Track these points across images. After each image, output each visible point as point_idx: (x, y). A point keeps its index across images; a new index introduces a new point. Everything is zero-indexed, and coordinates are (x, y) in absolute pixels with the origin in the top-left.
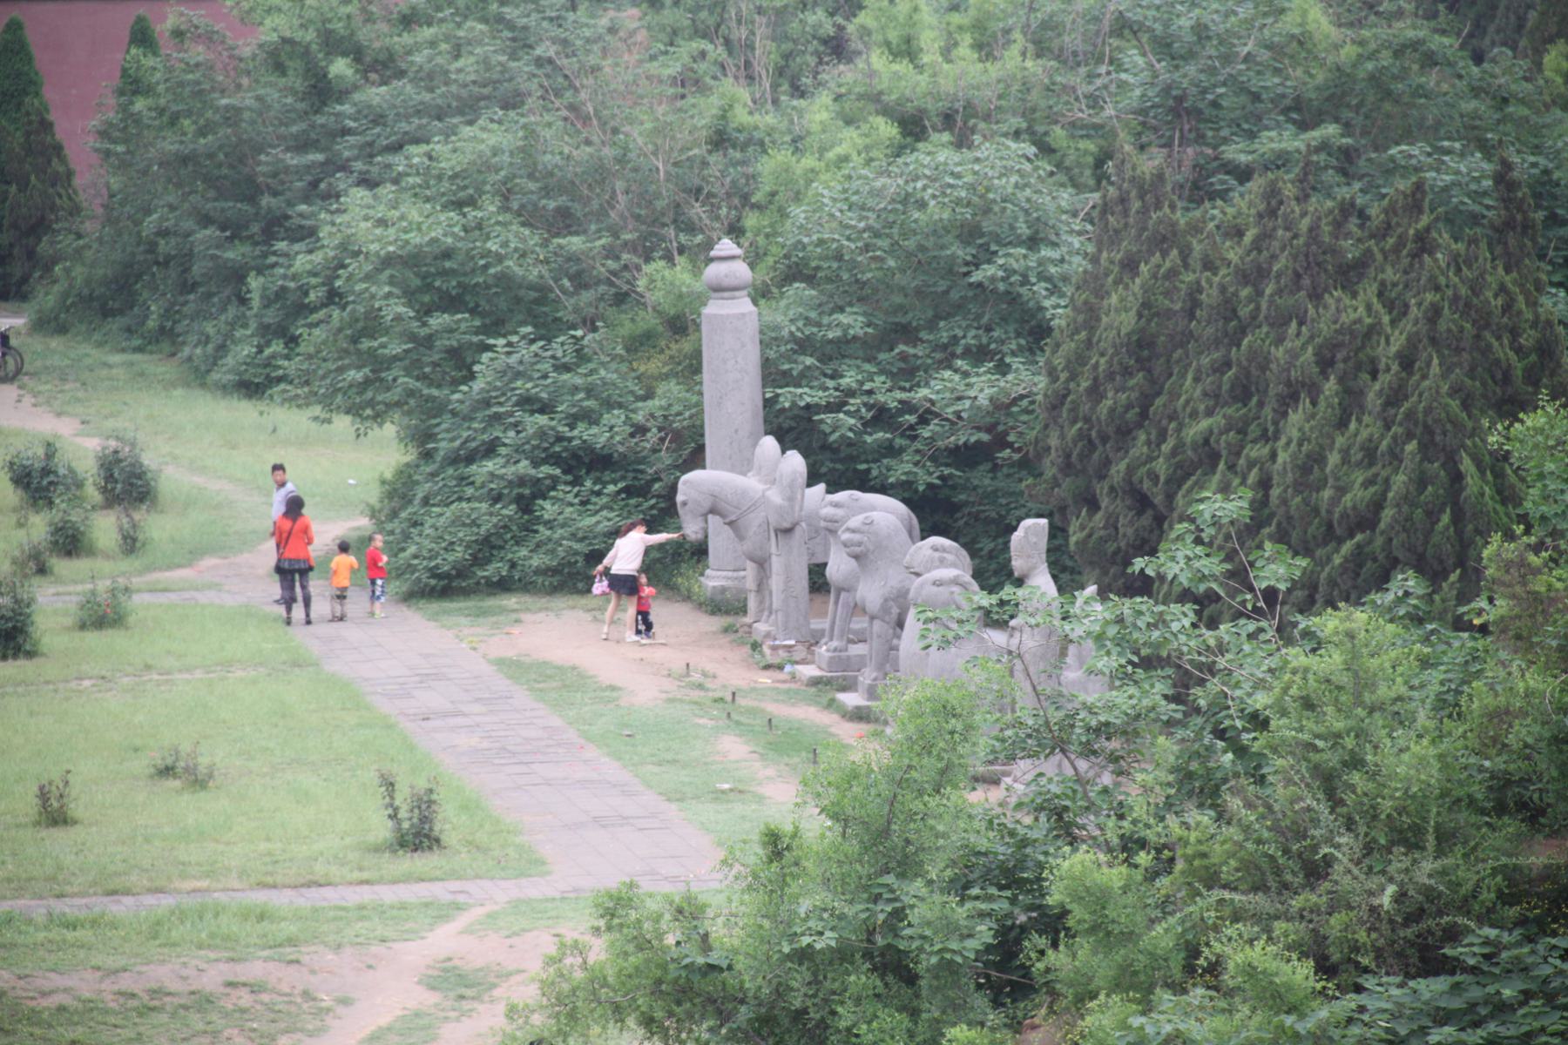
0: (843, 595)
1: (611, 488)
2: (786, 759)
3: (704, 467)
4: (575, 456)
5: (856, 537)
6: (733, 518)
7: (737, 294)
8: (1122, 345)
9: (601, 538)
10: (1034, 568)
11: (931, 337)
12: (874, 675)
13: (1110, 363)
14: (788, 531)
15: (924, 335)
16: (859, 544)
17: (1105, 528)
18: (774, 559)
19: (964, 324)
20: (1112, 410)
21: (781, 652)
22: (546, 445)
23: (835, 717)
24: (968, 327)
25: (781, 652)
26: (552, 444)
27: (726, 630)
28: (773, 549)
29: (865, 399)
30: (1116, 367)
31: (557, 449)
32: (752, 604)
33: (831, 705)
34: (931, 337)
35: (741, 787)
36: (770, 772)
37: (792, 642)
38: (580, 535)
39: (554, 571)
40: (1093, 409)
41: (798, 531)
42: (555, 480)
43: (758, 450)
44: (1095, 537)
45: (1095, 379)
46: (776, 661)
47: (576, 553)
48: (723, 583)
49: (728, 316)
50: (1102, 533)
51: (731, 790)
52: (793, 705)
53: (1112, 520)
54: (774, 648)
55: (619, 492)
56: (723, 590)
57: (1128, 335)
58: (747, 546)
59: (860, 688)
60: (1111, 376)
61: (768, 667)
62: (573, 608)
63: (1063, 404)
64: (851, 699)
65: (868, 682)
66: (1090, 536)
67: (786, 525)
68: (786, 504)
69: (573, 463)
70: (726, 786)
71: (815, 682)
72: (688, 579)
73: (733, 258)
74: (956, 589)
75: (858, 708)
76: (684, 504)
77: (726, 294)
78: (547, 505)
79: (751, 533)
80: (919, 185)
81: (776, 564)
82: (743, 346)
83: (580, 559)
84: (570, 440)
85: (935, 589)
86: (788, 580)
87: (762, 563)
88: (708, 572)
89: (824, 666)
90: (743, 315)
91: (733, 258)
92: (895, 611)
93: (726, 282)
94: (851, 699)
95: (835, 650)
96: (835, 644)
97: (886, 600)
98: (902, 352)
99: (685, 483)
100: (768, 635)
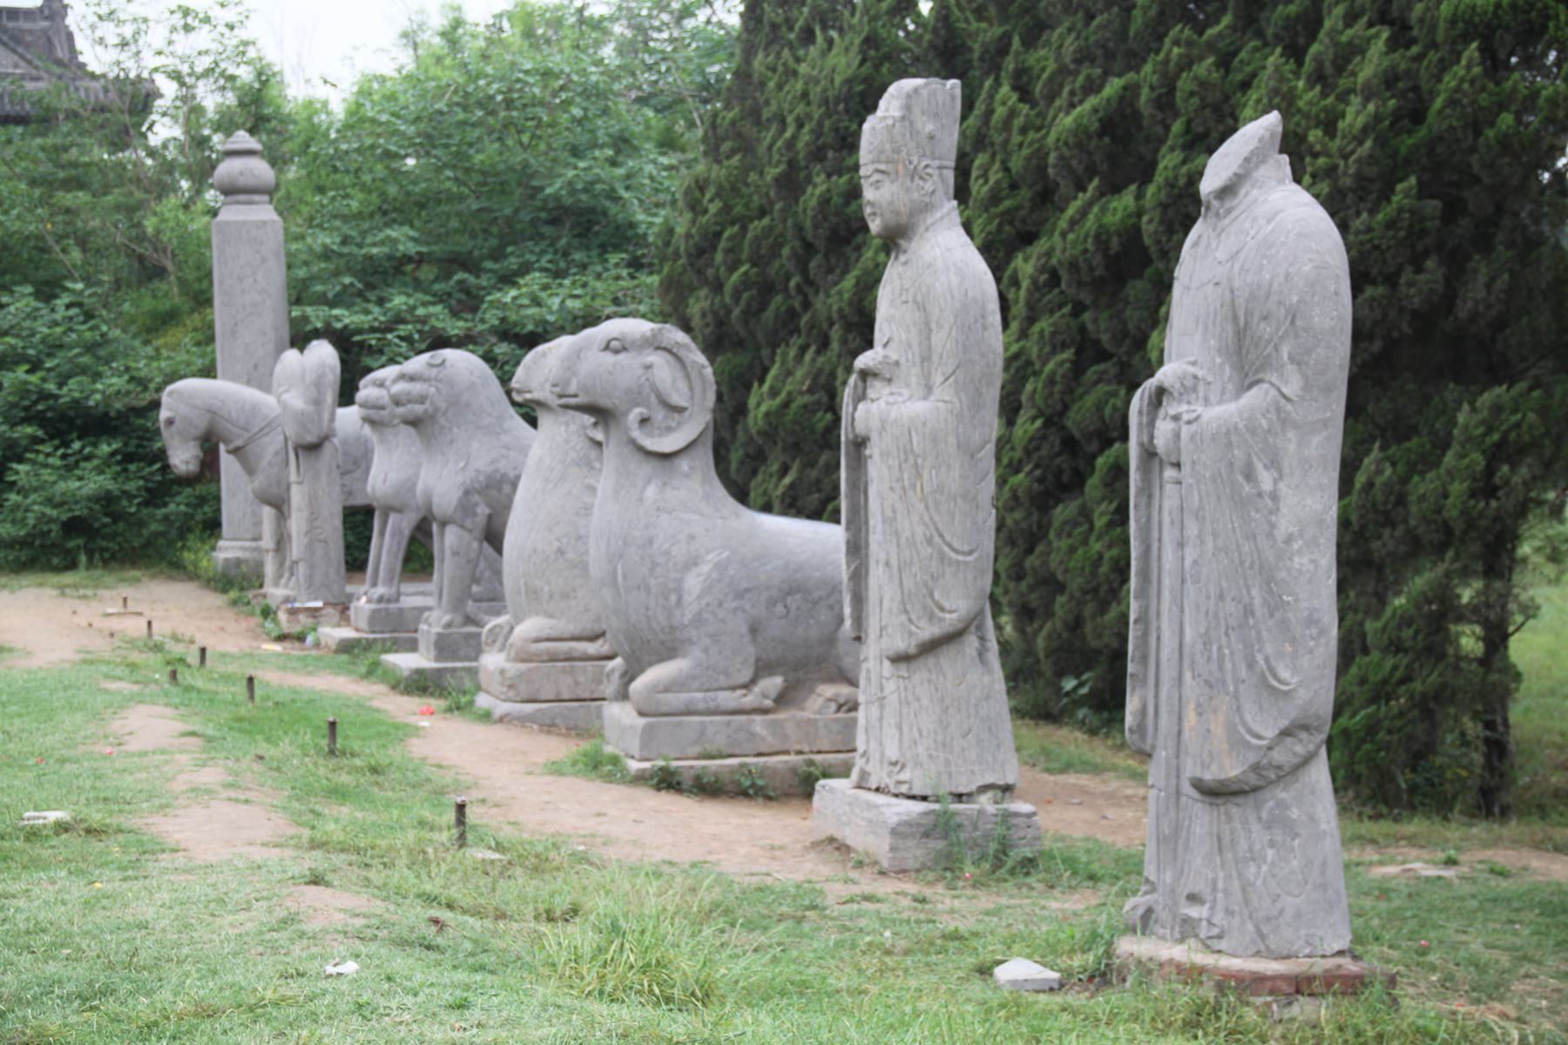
0: (392, 518)
1: (105, 449)
2: (263, 747)
3: (215, 377)
4: (63, 417)
5: (416, 388)
6: (239, 443)
7: (256, 198)
8: (837, 101)
9: (84, 503)
10: (927, 208)
11: (497, 266)
12: (447, 618)
13: (817, 133)
14: (314, 448)
15: (489, 265)
16: (422, 399)
17: (811, 391)
18: (294, 489)
19: (537, 250)
20: (825, 201)
21: (302, 617)
22: (26, 403)
23: (382, 688)
24: (543, 252)
25: (302, 617)
26: (35, 403)
27: (234, 603)
28: (293, 477)
29: (419, 327)
30: (828, 138)
31: (40, 407)
32: (269, 569)
33: (373, 671)
34: (497, 266)
35: (96, 817)
36: (210, 776)
37: (319, 604)
38: (58, 499)
39: (24, 543)
40: (722, 300)
41: (327, 449)
42: (36, 440)
43: (278, 368)
44: (794, 406)
45: (791, 164)
46: (297, 629)
47: (51, 520)
48: (239, 554)
49: (244, 223)
50: (806, 399)
51: (62, 828)
52: (309, 674)
53: (822, 380)
54: (293, 612)
55: (113, 454)
56: (238, 562)
57: (848, 81)
58: (259, 481)
59: (422, 646)
60: (818, 154)
61: (282, 638)
62: (41, 585)
63: (714, 248)
64: (405, 662)
65: (437, 629)
66: (786, 405)
67: (310, 439)
68: (310, 409)
69: (63, 426)
70: (53, 816)
71: (346, 647)
72: (196, 553)
73: (250, 153)
74: (657, 359)
75: (419, 672)
76: (170, 422)
77: (241, 197)
78: (22, 468)
79: (264, 463)
80: (482, 82)
81: (297, 497)
82: (264, 260)
83: (54, 527)
84: (57, 397)
85: (609, 358)
86: (313, 516)
87: (280, 505)
88: (221, 543)
89: (363, 624)
90: (264, 223)
91: (250, 153)
92: (483, 511)
93: (242, 181)
94: (405, 662)
95: (381, 600)
96: (381, 590)
97: (467, 493)
98: (460, 282)
99: (171, 394)
100: (287, 600)
